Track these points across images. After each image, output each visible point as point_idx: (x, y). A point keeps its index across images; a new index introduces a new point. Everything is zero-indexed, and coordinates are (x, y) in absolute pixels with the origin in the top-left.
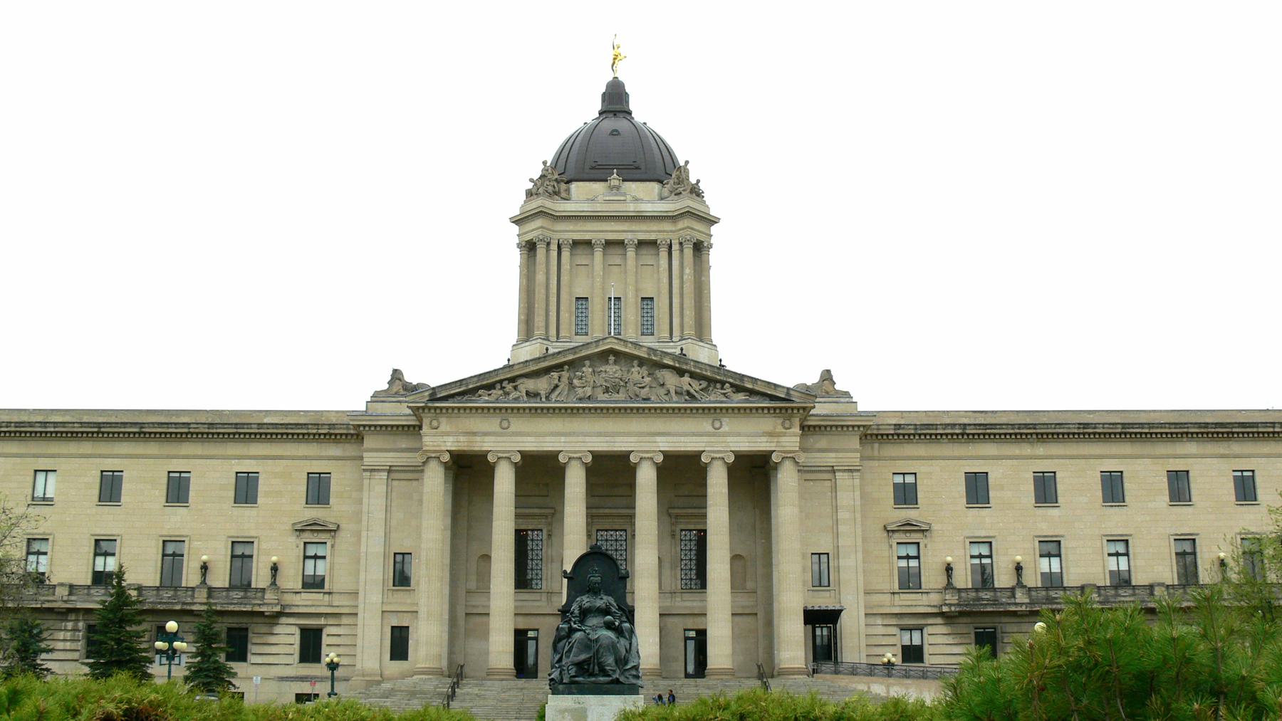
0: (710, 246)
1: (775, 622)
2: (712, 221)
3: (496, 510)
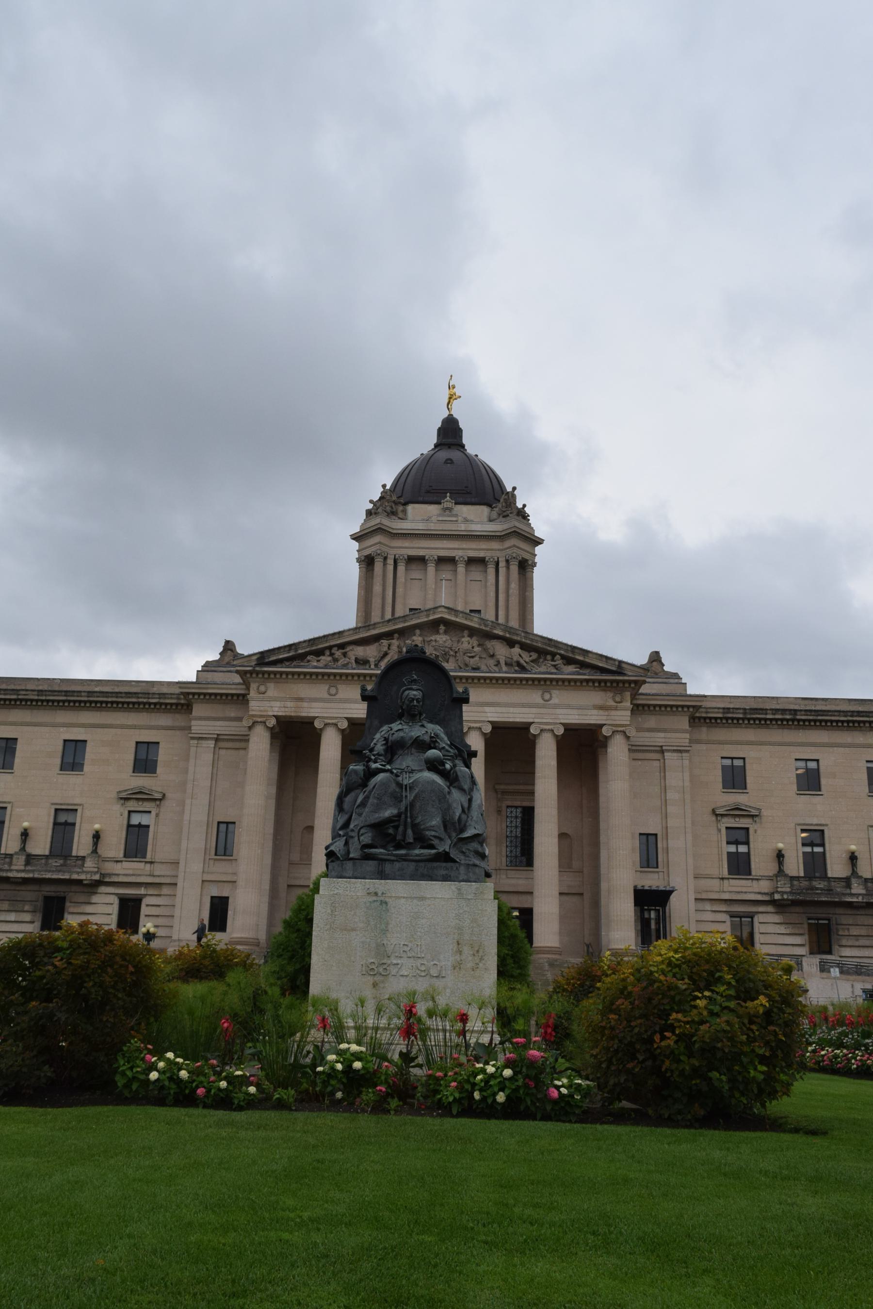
0: (534, 564)
1: (603, 901)
2: (538, 542)
3: (320, 790)
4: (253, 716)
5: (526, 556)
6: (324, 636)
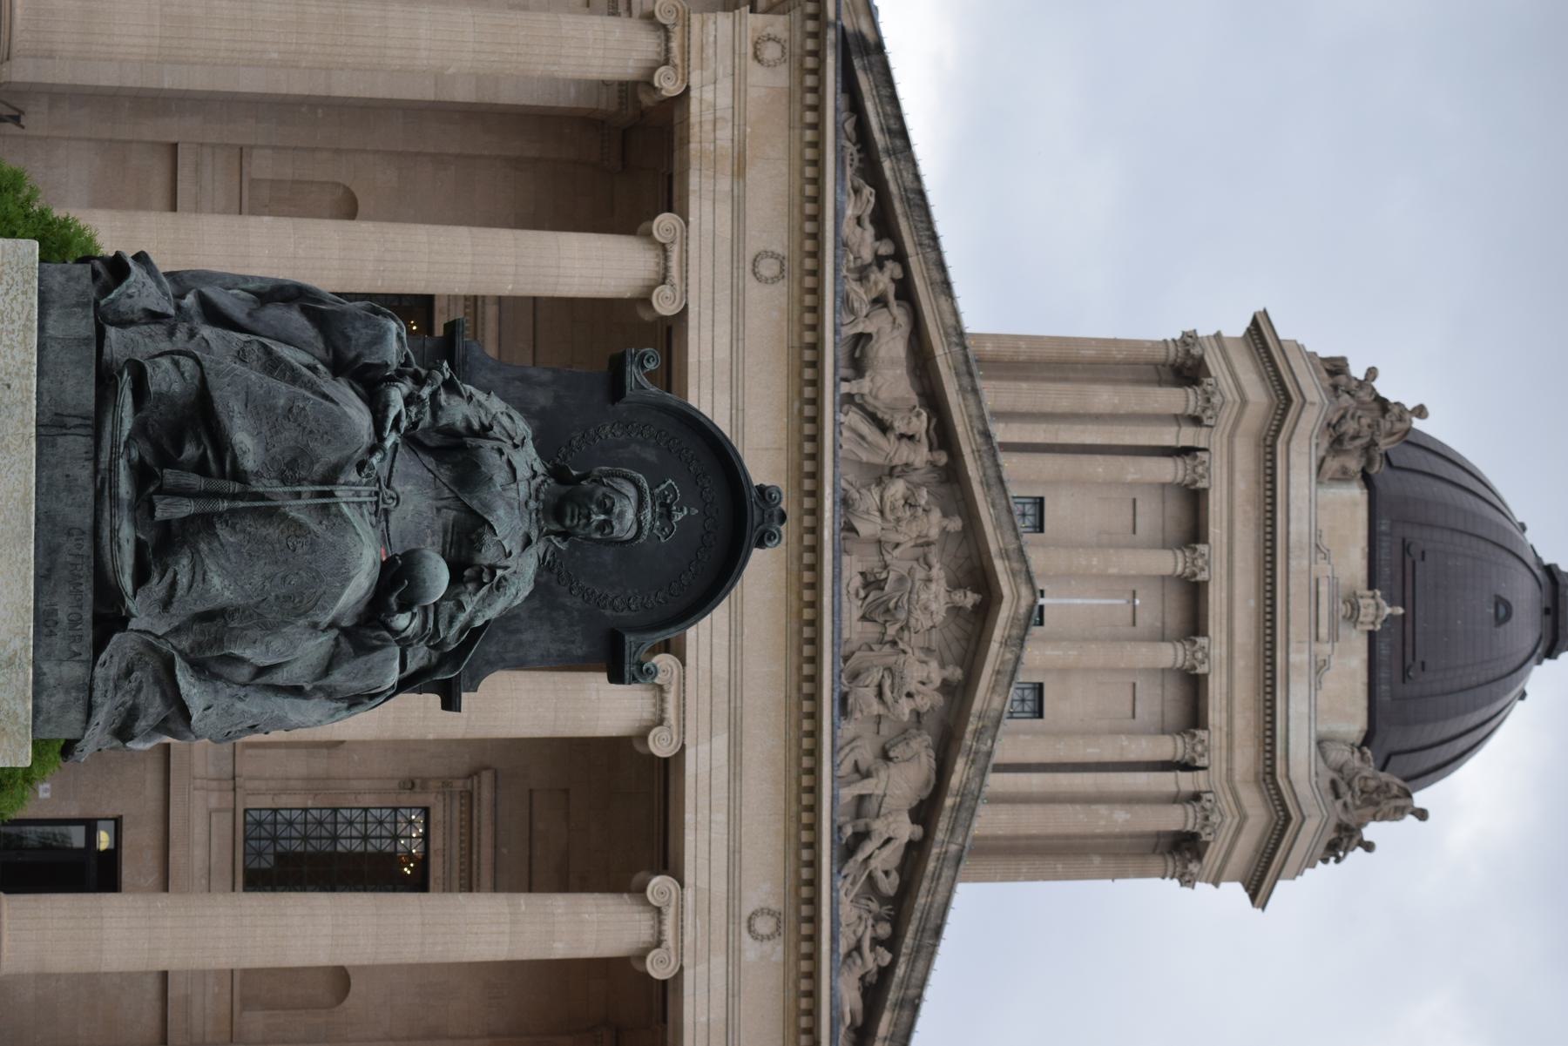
0: (1187, 880)
2: (1258, 890)
3: (462, 233)
4: (687, 26)
5: (1212, 856)
6: (934, 238)
